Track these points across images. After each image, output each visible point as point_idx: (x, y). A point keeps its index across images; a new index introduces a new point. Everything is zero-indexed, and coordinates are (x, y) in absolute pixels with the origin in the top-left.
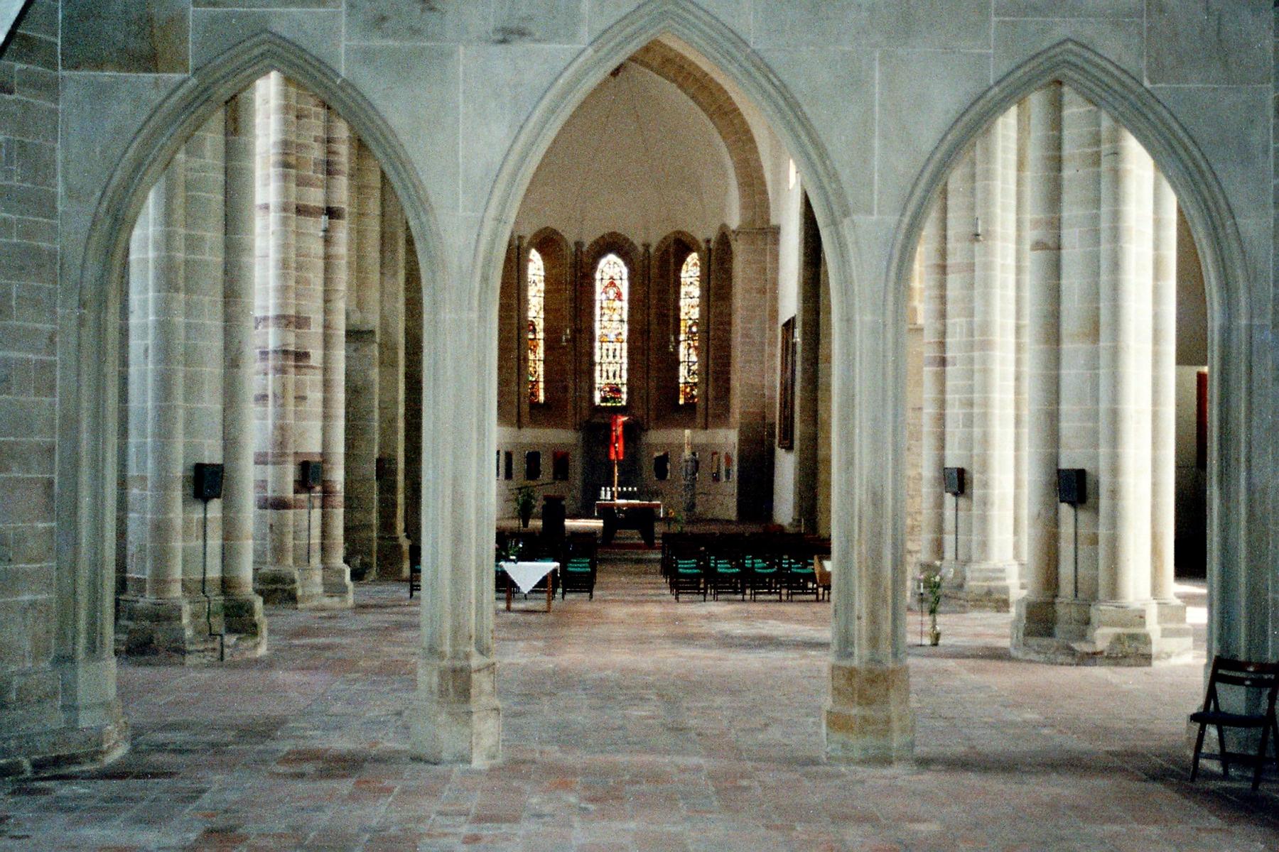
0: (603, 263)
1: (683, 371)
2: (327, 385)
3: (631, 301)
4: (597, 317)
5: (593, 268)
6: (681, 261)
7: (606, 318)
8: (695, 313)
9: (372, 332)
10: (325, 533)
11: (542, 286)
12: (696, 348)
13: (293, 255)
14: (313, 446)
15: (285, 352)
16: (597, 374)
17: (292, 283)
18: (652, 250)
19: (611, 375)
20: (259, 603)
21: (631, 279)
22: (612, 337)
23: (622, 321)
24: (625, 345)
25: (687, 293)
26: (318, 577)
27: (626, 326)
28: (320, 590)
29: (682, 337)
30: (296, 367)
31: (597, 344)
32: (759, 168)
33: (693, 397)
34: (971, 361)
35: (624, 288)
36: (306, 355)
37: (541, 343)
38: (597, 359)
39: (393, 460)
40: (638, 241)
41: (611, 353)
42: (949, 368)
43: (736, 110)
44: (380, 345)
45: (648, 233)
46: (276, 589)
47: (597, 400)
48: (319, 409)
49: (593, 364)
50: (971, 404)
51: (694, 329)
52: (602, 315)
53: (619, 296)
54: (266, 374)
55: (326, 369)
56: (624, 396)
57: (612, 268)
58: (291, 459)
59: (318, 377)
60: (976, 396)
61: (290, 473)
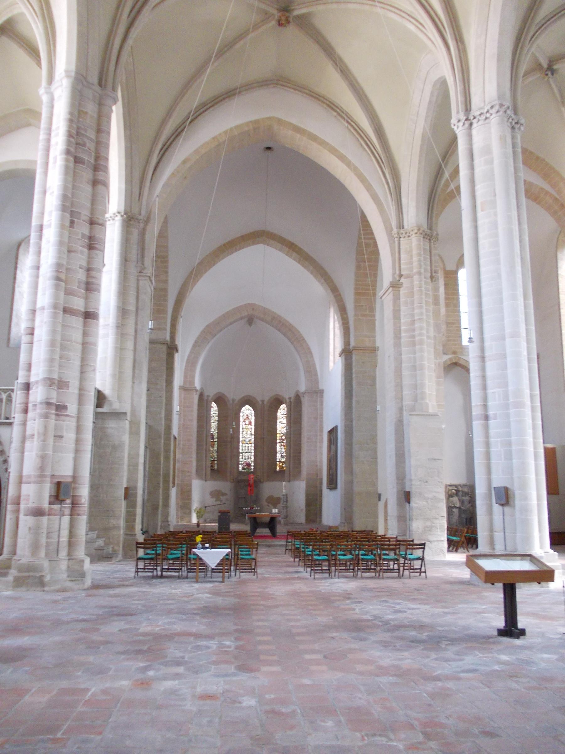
0: (243, 409)
1: (278, 456)
2: (79, 429)
3: (255, 426)
4: (241, 433)
5: (239, 411)
6: (278, 408)
7: (245, 433)
8: (284, 430)
9: (125, 414)
10: (72, 534)
11: (217, 418)
12: (284, 446)
13: (59, 338)
14: (65, 471)
15: (48, 404)
16: (240, 457)
17: (57, 357)
18: (265, 403)
19: (247, 458)
20: (87, 560)
21: (256, 416)
22: (247, 441)
23: (251, 434)
24: (253, 445)
25: (280, 422)
26: (64, 565)
27: (253, 437)
28: (65, 576)
29: (278, 441)
30: (57, 415)
31: (241, 444)
32: (314, 365)
33: (283, 467)
34: (508, 416)
35: (253, 420)
36: (65, 407)
37: (216, 443)
38: (241, 451)
39: (135, 488)
40: (259, 399)
41: (247, 448)
42: (491, 422)
43: (304, 339)
44: (131, 422)
45: (264, 395)
46: (29, 577)
47: (240, 469)
48: (72, 446)
49: (239, 453)
50: (509, 444)
51: (284, 438)
52: (243, 432)
53: (250, 424)
54: (35, 420)
55: (79, 418)
56: (253, 467)
57: (247, 411)
58: (48, 479)
59: (73, 423)
60: (513, 438)
61: (47, 489)
